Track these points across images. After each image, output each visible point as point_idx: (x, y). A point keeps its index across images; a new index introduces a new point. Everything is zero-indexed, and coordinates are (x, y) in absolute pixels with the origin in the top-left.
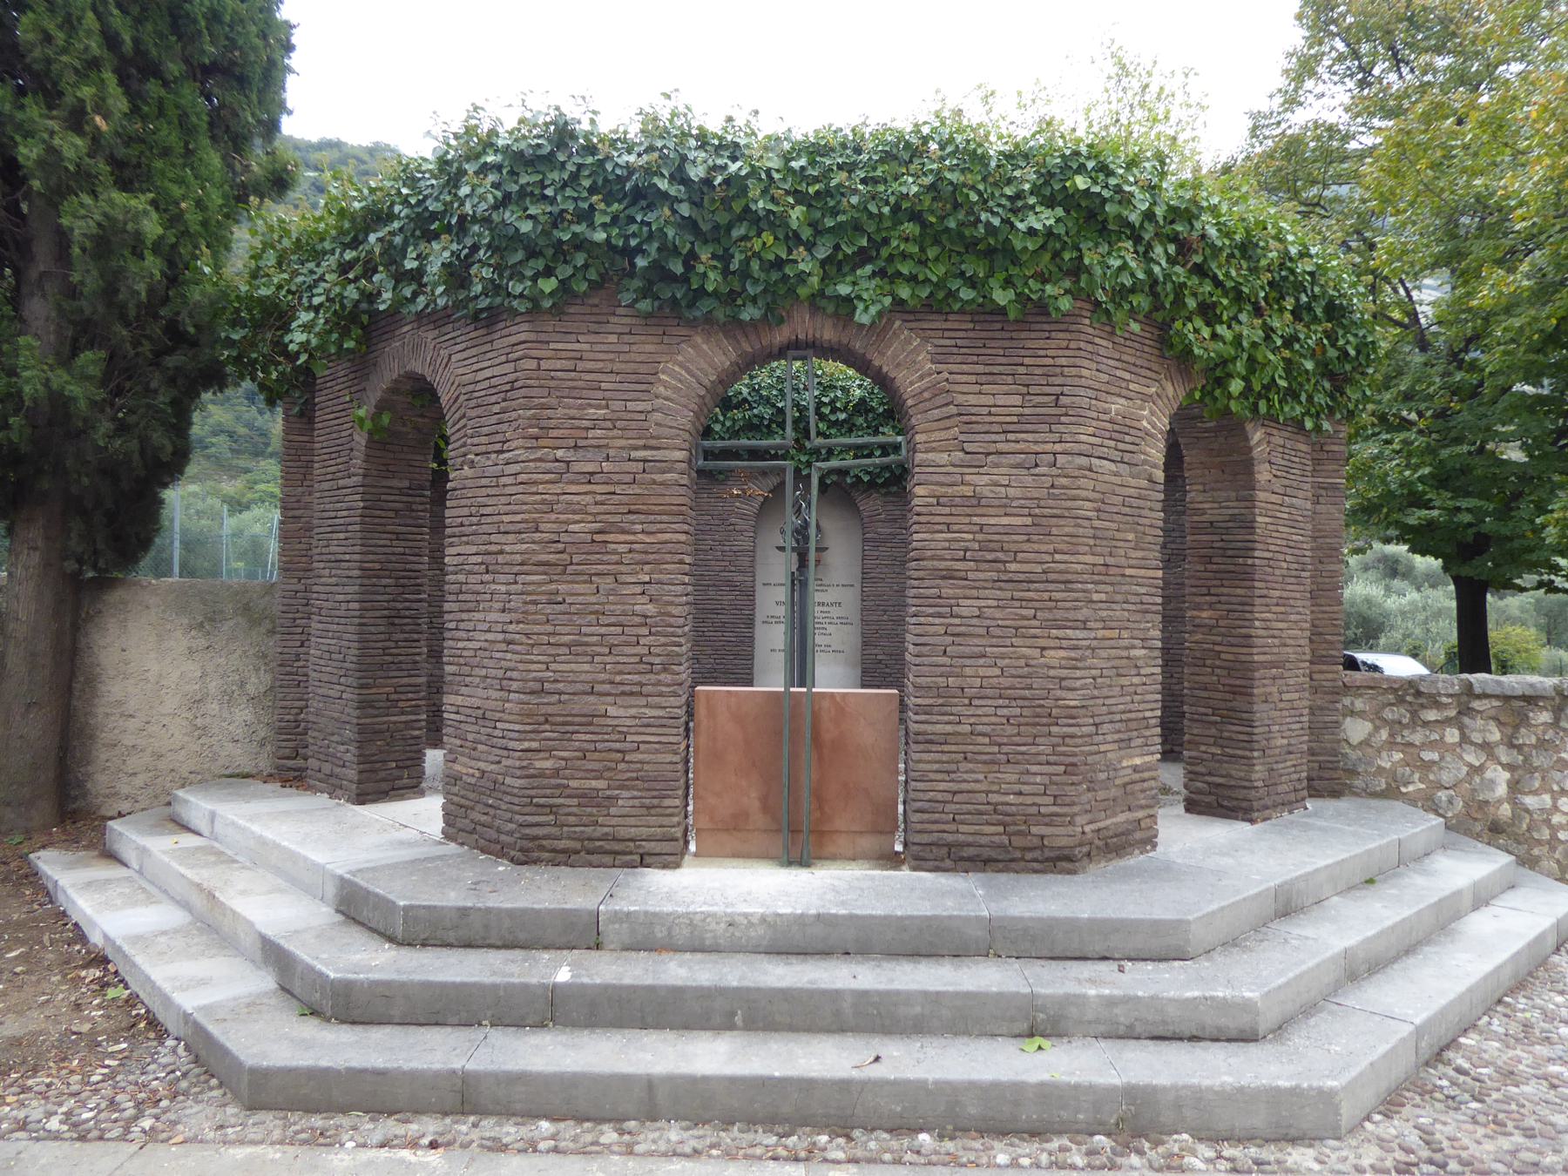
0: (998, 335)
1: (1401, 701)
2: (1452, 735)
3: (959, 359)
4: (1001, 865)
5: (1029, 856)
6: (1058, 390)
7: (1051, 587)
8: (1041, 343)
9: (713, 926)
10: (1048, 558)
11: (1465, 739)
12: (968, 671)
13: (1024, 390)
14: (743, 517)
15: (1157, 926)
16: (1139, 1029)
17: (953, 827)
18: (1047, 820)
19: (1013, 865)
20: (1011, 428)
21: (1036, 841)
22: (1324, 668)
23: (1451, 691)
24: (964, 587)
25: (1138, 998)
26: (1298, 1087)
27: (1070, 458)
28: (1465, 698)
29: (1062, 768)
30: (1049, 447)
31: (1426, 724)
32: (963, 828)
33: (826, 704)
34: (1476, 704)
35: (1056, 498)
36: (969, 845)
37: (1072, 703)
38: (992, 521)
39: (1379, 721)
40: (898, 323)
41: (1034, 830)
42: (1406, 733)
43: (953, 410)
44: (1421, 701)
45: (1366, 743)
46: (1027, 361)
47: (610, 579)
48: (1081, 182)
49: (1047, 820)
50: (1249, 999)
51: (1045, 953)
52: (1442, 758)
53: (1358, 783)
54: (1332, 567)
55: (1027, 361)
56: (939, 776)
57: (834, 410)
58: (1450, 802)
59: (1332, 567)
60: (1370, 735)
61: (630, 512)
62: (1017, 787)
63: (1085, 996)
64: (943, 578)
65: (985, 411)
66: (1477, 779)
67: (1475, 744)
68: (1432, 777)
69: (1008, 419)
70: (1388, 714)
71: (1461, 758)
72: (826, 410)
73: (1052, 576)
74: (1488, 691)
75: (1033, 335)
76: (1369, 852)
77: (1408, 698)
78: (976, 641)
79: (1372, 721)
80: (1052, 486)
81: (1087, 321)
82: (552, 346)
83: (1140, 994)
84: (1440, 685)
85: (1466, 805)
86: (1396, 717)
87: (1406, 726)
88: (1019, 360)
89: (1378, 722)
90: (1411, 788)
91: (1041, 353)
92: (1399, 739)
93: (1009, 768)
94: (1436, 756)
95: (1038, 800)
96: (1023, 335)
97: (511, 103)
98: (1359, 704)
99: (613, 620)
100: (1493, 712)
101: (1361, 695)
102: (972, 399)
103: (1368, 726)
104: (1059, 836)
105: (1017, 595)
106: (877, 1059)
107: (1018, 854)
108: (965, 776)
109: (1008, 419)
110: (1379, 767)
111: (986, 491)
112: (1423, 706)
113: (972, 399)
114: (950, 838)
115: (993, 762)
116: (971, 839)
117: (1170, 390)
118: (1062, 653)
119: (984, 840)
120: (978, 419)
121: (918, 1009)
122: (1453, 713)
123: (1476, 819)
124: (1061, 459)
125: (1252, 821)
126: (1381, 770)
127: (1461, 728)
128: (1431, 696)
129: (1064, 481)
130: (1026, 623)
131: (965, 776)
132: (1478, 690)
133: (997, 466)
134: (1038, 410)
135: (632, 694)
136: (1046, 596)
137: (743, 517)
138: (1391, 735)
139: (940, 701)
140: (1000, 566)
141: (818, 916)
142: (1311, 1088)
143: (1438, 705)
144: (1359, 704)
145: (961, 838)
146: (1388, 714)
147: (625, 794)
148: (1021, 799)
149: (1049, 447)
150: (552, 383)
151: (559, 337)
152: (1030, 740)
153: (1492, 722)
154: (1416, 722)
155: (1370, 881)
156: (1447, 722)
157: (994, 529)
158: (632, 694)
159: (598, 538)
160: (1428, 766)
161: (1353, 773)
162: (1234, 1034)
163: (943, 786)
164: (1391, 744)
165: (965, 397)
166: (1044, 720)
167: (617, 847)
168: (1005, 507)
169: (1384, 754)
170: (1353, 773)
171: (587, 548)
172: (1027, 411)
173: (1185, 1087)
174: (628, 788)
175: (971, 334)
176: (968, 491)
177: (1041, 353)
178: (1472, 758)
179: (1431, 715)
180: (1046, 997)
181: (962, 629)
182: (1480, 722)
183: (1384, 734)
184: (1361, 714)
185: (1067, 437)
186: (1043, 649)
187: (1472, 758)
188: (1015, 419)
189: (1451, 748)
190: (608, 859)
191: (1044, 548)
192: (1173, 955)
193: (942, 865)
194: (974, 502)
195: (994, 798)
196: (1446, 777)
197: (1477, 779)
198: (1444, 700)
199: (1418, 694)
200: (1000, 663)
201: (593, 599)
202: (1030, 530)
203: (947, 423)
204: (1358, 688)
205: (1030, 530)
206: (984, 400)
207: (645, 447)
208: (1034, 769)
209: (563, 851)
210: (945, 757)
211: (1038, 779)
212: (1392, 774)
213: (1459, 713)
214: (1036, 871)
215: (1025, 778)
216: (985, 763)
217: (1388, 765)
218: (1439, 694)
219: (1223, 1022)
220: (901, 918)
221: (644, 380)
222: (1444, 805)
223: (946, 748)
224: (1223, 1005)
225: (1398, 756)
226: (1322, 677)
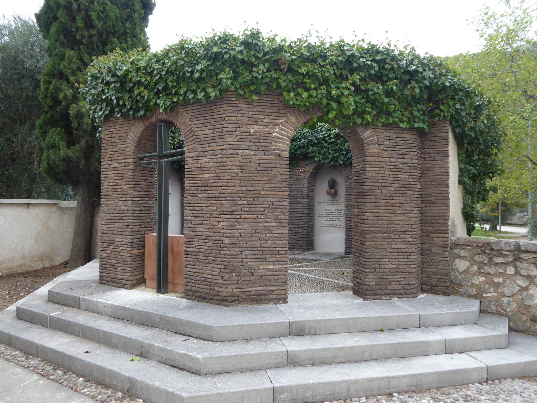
0: (206, 109)
1: (483, 252)
2: (511, 271)
3: (196, 119)
4: (207, 300)
5: (215, 298)
6: (222, 126)
7: (221, 199)
8: (218, 110)
9: (101, 306)
10: (220, 188)
11: (517, 273)
12: (198, 230)
13: (213, 127)
14: (304, 179)
15: (205, 327)
16: (168, 362)
17: (194, 285)
18: (219, 285)
19: (210, 301)
20: (210, 142)
21: (216, 293)
22: (439, 235)
23: (508, 249)
24: (197, 200)
25: (168, 350)
26: (173, 393)
27: (227, 151)
28: (517, 252)
29: (224, 266)
30: (220, 147)
31: (497, 264)
32: (197, 286)
33: (175, 240)
34: (523, 256)
35: (223, 166)
36: (199, 292)
37: (227, 242)
38: (205, 176)
39: (473, 262)
40: (181, 110)
41: (216, 289)
42: (486, 268)
43: (194, 137)
44: (493, 253)
45: (466, 271)
46: (214, 117)
47: (117, 199)
48: (215, 49)
49: (219, 285)
50: (198, 358)
51: (174, 331)
52: (504, 281)
53: (462, 290)
54: (442, 189)
55: (214, 117)
56: (190, 266)
57: (330, 138)
58: (509, 303)
59: (442, 189)
60: (469, 268)
61: (122, 179)
62: (211, 272)
63: (154, 346)
64: (192, 197)
65: (202, 136)
66: (525, 294)
67: (523, 276)
68: (500, 290)
69: (209, 139)
70: (477, 258)
71: (516, 283)
72: (327, 139)
73: (221, 195)
74: (529, 249)
75: (217, 107)
76: (385, 318)
77: (487, 251)
78: (200, 219)
79: (469, 261)
80: (222, 162)
81: (234, 99)
82: (108, 131)
83: (169, 348)
84: (503, 245)
85: (519, 307)
86: (481, 260)
87: (486, 265)
88: (212, 117)
89: (472, 262)
90: (489, 295)
91: (218, 113)
92: (483, 271)
93: (209, 265)
94: (501, 280)
95: (217, 278)
96: (214, 107)
97: (380, 41)
98: (463, 253)
99: (117, 212)
100: (532, 260)
101: (464, 249)
102: (199, 133)
103: (467, 263)
104: (224, 292)
105: (212, 202)
106: (132, 360)
107: (211, 297)
108: (197, 267)
109: (209, 139)
110: (473, 283)
111: (203, 165)
112: (495, 256)
113: (199, 133)
114: (193, 288)
115: (204, 263)
116: (199, 290)
117: (293, 119)
118: (224, 224)
119: (202, 290)
120: (201, 140)
121: (116, 340)
122: (510, 259)
123: (523, 314)
124: (224, 151)
125: (365, 299)
126: (473, 285)
127: (516, 267)
128: (498, 251)
129: (224, 159)
130: (214, 212)
131: (197, 267)
132: (523, 249)
133: (206, 156)
134: (217, 134)
135: (121, 234)
136: (219, 202)
137: (304, 179)
138: (479, 268)
139: (190, 240)
140: (207, 192)
141: (122, 307)
142: (177, 394)
143: (503, 256)
144: (463, 253)
145: (196, 289)
146: (477, 258)
147: (119, 265)
148: (212, 277)
149: (220, 147)
150: (107, 142)
151: (108, 128)
152: (215, 255)
153: (532, 265)
154: (491, 263)
155: (382, 330)
156: (508, 264)
157: (205, 179)
158: (121, 234)
159: (115, 187)
160: (497, 285)
161: (460, 285)
162: (194, 371)
163: (191, 270)
164: (479, 273)
165: (198, 132)
166: (219, 248)
167: (118, 281)
168: (209, 169)
169: (475, 277)
170: (460, 285)
171: (113, 190)
172: (214, 135)
173: (143, 382)
174: (121, 264)
175: (200, 110)
176: (198, 165)
177: (218, 113)
178: (523, 283)
179: (499, 260)
180: (145, 343)
181: (196, 215)
182: (525, 265)
183: (475, 268)
184: (464, 258)
185: (226, 143)
186: (219, 222)
187: (523, 283)
188: (211, 138)
189: (510, 277)
190: (116, 285)
191: (219, 185)
192: (209, 339)
193: (192, 298)
194: (200, 169)
195: (205, 276)
196: (506, 291)
197: (525, 294)
198: (505, 253)
199: (492, 249)
200: (207, 227)
201: (114, 205)
202: (215, 178)
203: (193, 142)
204: (462, 245)
205: (215, 178)
206: (203, 133)
207: (125, 159)
208: (216, 266)
209: (108, 281)
210: (192, 260)
211: (217, 270)
212: (479, 287)
213: (515, 260)
214: (217, 304)
215: (214, 269)
216: (202, 263)
217: (477, 283)
218: (503, 250)
219: (191, 365)
220: (140, 311)
221: (125, 138)
222: (505, 305)
223: (192, 256)
224: (191, 358)
225: (482, 279)
226: (438, 239)
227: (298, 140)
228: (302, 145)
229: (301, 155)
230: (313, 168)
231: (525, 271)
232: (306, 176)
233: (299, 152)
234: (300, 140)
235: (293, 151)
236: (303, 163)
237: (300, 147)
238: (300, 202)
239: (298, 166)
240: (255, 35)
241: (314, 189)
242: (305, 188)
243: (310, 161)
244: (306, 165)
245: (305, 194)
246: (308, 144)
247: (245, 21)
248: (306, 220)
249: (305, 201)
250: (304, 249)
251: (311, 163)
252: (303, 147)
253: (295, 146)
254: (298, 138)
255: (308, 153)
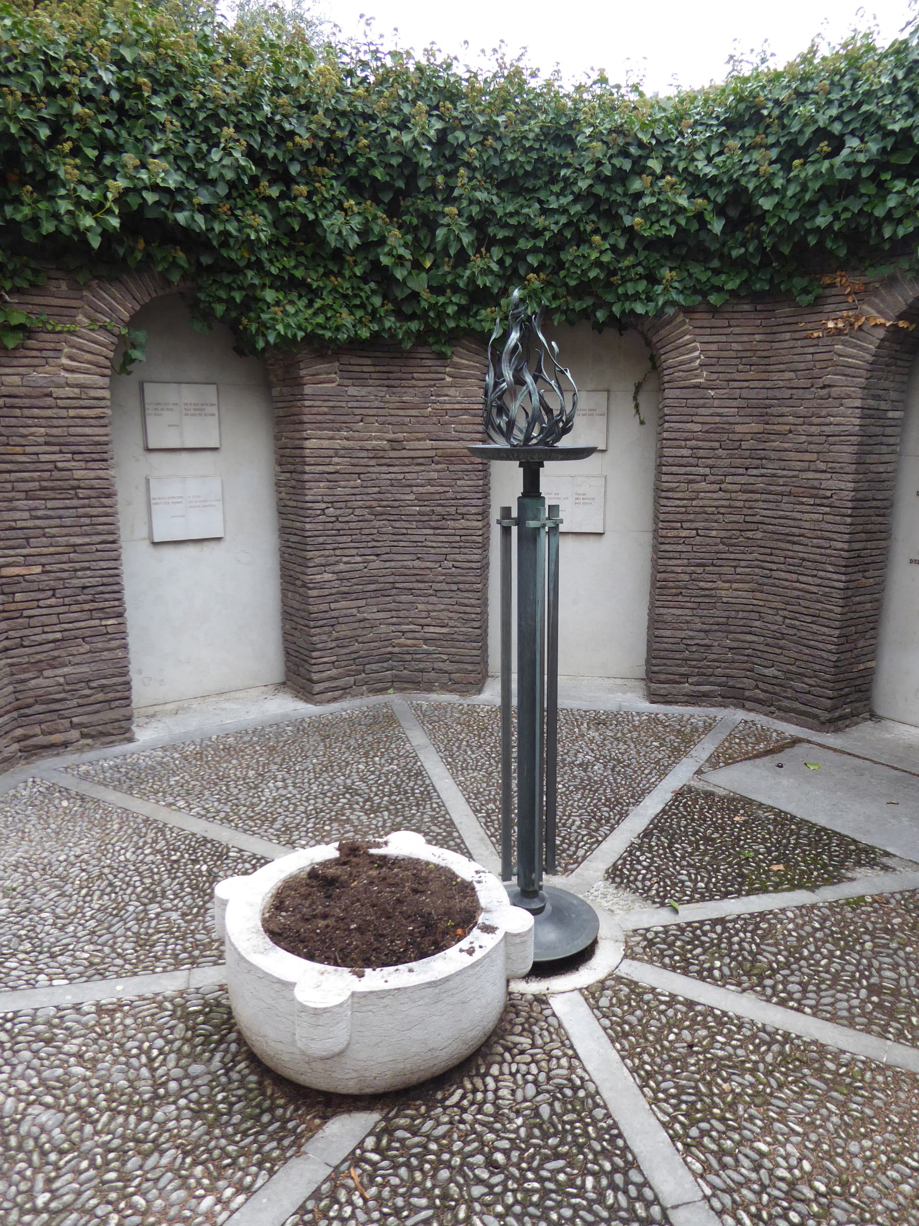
14: (846, 371)
137: (846, 371)
227: (824, 146)
228: (846, 174)
229: (838, 235)
230: (903, 307)
231: (36, 1112)
232: (858, 354)
233: (821, 221)
234: (838, 144)
235: (792, 218)
236: (845, 282)
237: (835, 191)
238: (814, 491)
239: (819, 301)
240: (515, 76)
241: (901, 425)
242: (847, 418)
243: (886, 271)
244: (865, 293)
245: (845, 453)
246: (880, 164)
247: (466, 42)
248: (839, 580)
249: (842, 486)
250: (815, 717)
251: (891, 282)
252: (847, 189)
253: (804, 188)
254: (822, 133)
255: (879, 223)
